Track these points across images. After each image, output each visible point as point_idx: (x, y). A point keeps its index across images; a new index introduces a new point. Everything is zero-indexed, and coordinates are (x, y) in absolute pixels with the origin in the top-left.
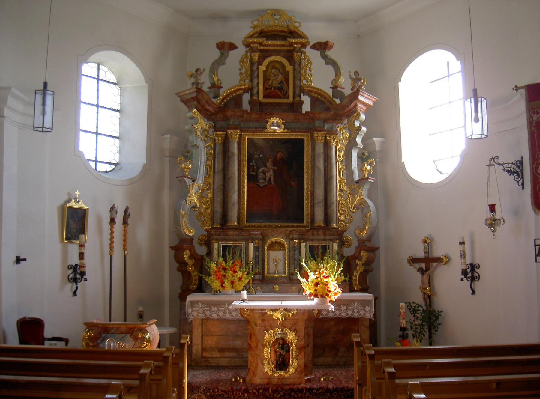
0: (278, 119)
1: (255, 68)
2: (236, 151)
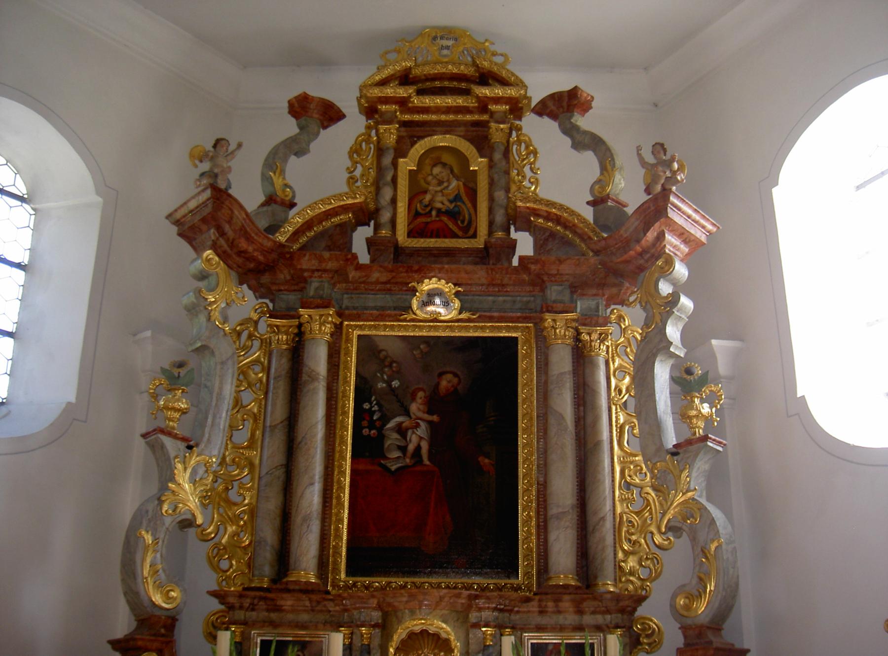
0: (443, 281)
1: (387, 160)
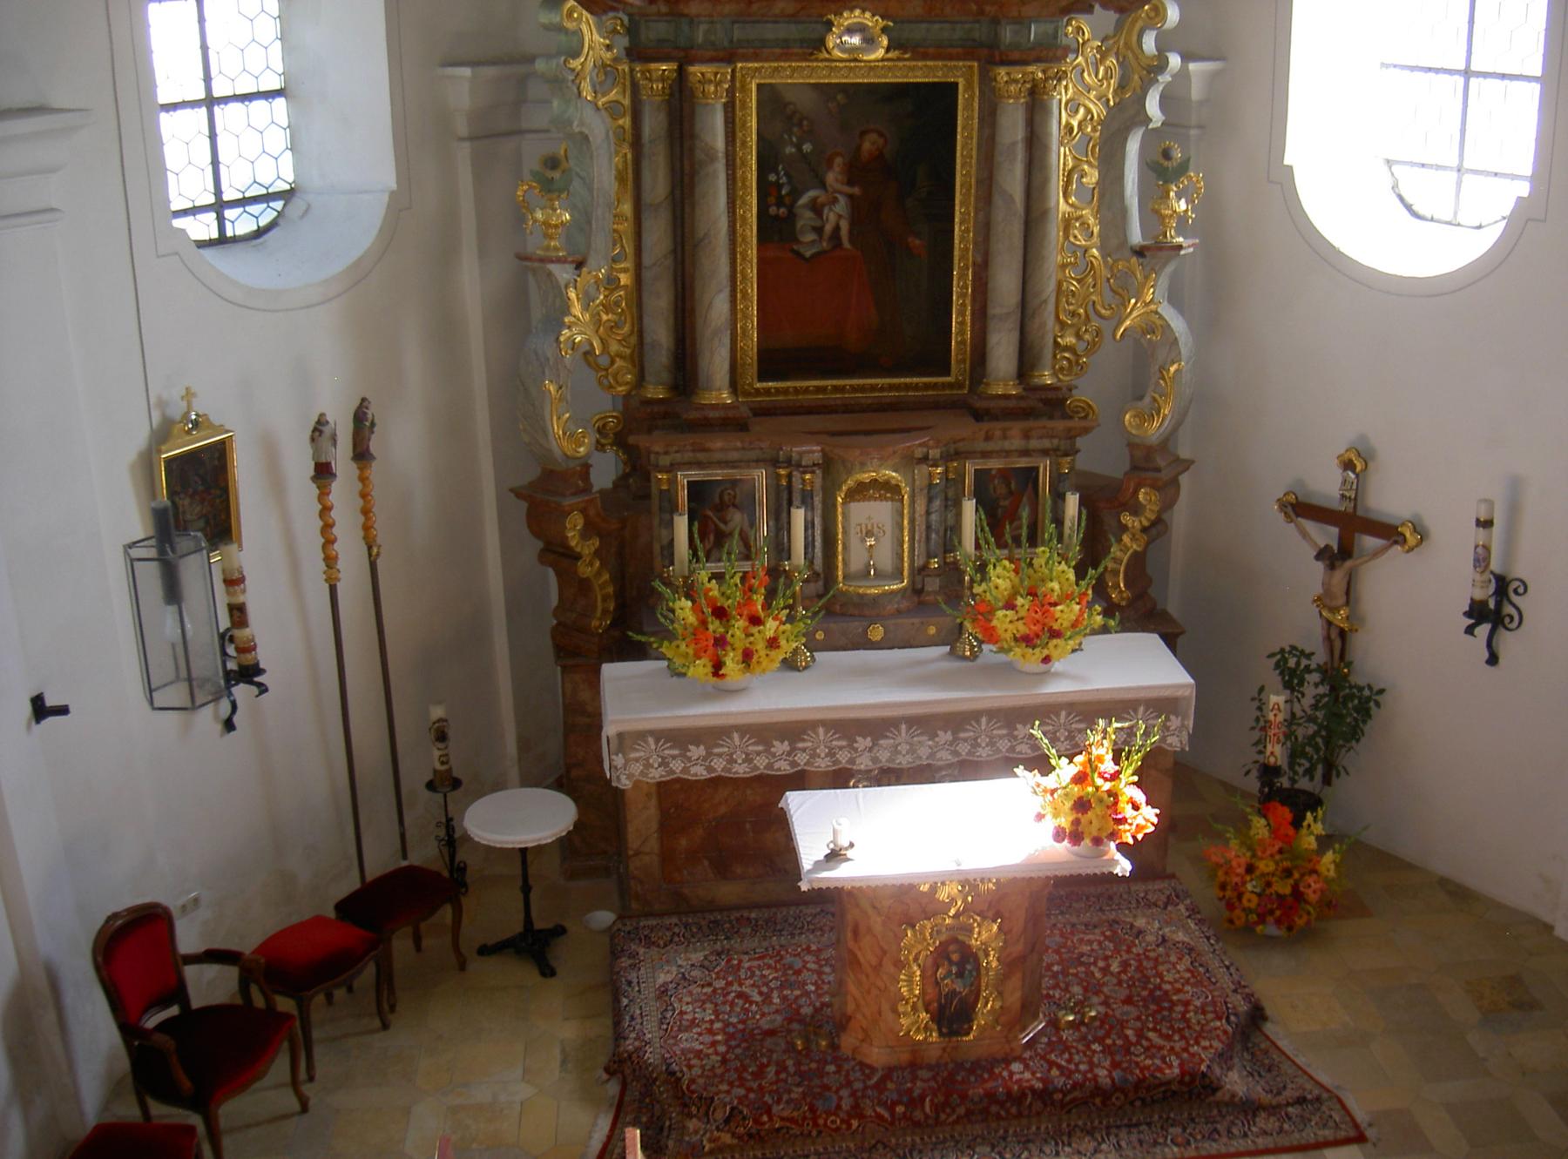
0: (868, 15)
2: (720, 143)
